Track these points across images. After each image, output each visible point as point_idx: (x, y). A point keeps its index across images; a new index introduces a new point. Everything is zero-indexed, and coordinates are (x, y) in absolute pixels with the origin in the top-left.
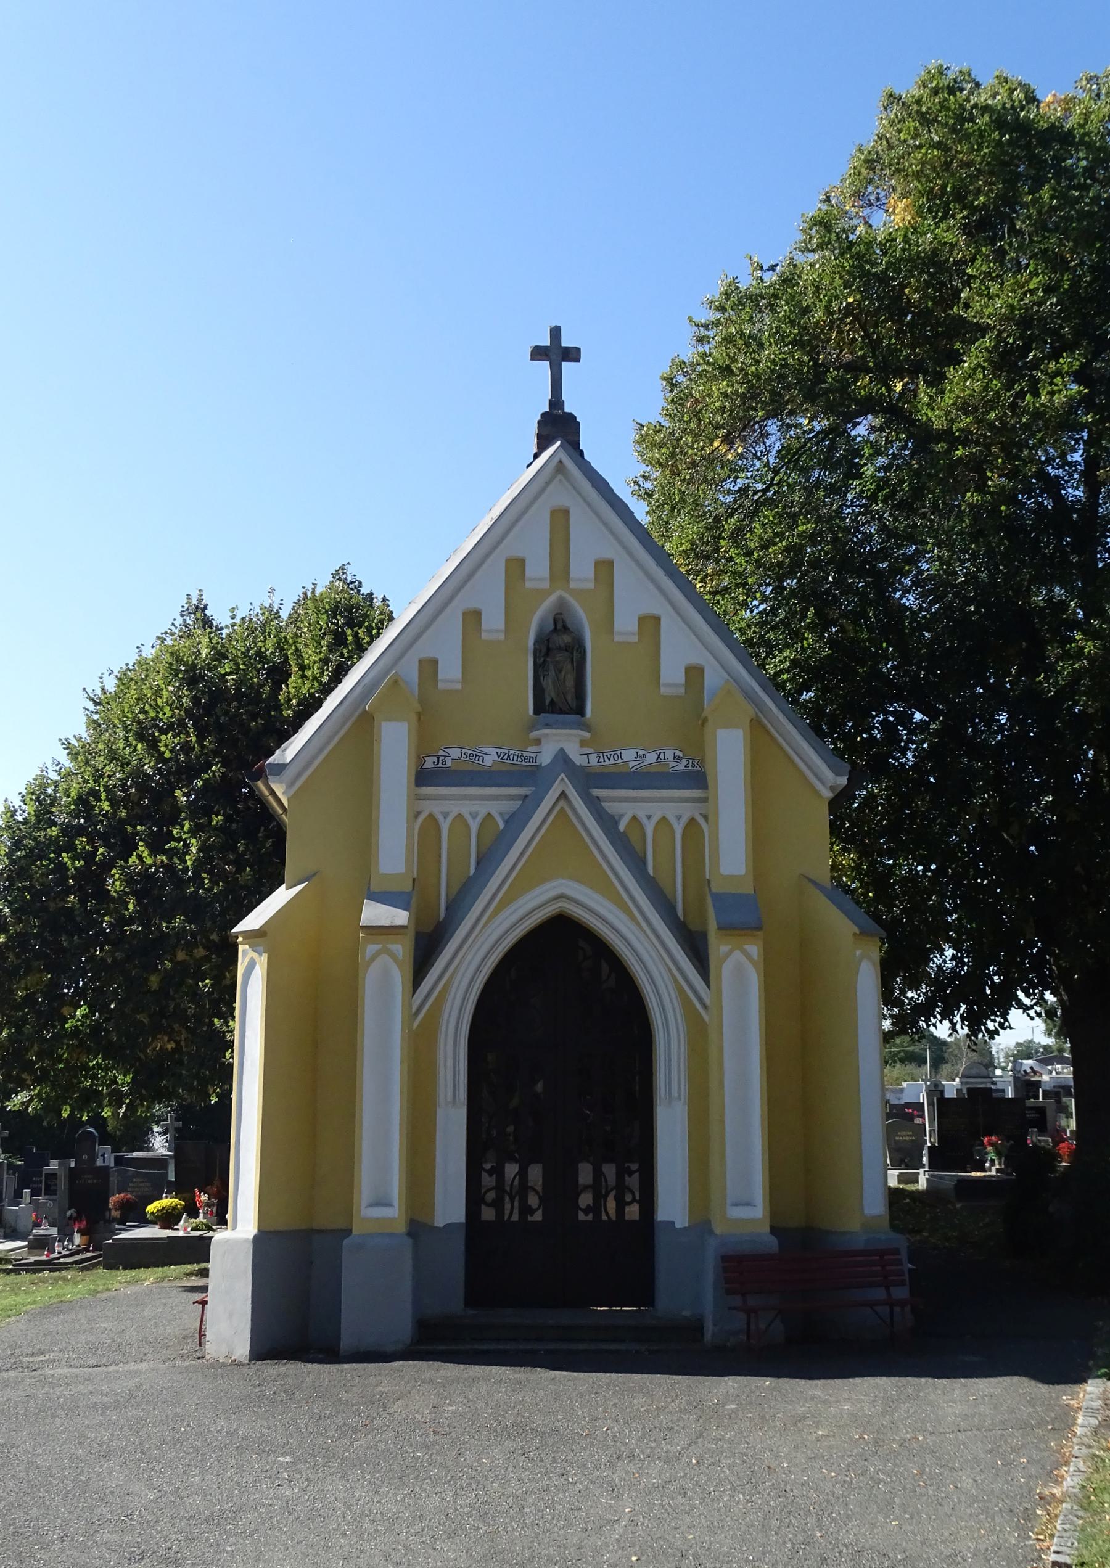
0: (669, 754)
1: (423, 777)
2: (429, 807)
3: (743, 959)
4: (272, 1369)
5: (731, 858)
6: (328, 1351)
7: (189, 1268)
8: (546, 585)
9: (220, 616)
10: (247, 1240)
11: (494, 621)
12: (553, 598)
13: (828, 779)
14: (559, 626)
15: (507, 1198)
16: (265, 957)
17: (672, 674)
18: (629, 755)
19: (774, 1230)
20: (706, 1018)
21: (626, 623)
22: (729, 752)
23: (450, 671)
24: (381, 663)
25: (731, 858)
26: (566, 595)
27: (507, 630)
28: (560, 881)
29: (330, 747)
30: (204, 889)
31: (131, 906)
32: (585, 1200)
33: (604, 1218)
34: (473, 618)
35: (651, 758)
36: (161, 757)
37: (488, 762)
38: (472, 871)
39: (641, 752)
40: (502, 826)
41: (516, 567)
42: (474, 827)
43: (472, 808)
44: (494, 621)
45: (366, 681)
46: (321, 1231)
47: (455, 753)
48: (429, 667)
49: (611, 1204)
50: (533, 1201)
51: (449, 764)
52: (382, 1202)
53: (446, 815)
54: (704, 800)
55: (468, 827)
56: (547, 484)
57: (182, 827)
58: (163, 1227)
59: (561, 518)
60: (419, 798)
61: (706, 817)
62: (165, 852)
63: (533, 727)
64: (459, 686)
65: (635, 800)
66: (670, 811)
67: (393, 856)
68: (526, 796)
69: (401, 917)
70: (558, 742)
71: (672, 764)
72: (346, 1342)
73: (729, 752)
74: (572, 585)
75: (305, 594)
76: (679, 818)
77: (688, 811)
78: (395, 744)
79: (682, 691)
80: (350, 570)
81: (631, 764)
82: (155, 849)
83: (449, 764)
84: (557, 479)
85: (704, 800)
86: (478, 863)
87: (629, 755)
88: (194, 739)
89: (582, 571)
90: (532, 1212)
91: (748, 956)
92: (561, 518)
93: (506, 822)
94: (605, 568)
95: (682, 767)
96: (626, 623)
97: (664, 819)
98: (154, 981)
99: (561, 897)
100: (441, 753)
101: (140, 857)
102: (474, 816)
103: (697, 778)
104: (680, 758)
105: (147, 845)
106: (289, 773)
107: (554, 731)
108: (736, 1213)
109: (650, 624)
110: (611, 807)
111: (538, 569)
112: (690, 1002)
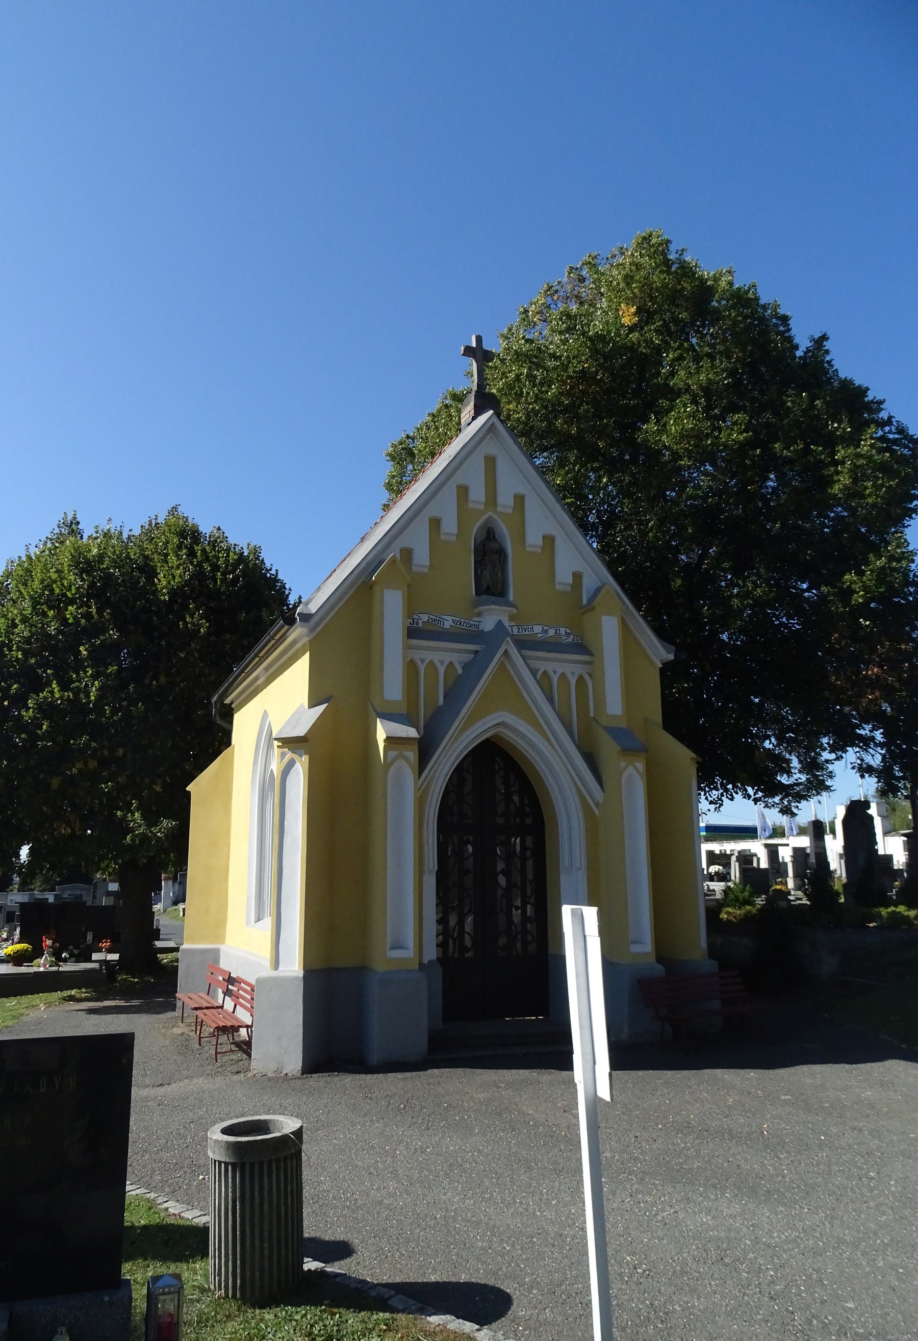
0: (563, 631)
1: (413, 632)
2: (417, 655)
3: (635, 772)
4: (318, 1080)
5: (614, 705)
6: (358, 1064)
7: (59, 994)
8: (482, 507)
9: (87, 529)
10: (297, 978)
11: (450, 526)
12: (486, 516)
13: (660, 653)
14: (491, 537)
15: (451, 940)
16: (305, 758)
17: (564, 577)
18: (538, 629)
19: (659, 959)
20: (597, 812)
21: (534, 538)
22: (609, 630)
23: (422, 558)
24: (378, 548)
25: (614, 705)
26: (495, 517)
27: (458, 536)
28: (501, 713)
29: (340, 604)
30: (106, 718)
31: (44, 727)
32: (502, 941)
33: (514, 953)
34: (435, 523)
35: (552, 632)
36: (64, 621)
37: (447, 625)
38: (441, 701)
39: (545, 628)
40: (460, 671)
41: (463, 492)
42: (442, 670)
43: (444, 657)
44: (450, 526)
45: (369, 558)
46: (337, 969)
47: (425, 618)
48: (407, 554)
49: (519, 945)
50: (468, 942)
51: (420, 625)
52: (397, 946)
53: (422, 661)
54: (590, 663)
55: (437, 671)
56: (482, 439)
57: (86, 672)
58: (15, 965)
59: (491, 462)
60: (410, 647)
61: (590, 675)
62: (72, 690)
63: (476, 604)
64: (426, 570)
65: (546, 659)
66: (567, 669)
67: (393, 688)
68: (476, 652)
69: (412, 732)
70: (491, 618)
71: (565, 638)
72: (374, 1058)
73: (609, 630)
74: (499, 509)
75: (151, 521)
76: (573, 674)
77: (579, 670)
78: (392, 607)
79: (569, 589)
80: (180, 509)
81: (539, 636)
82: (64, 687)
83: (420, 625)
84: (488, 437)
85: (590, 663)
86: (445, 697)
87: (538, 629)
88: (95, 611)
89: (505, 500)
90: (467, 950)
91: (637, 770)
92: (491, 462)
93: (463, 668)
94: (520, 500)
95: (570, 640)
96: (534, 538)
97: (563, 674)
98: (55, 782)
99: (502, 724)
100: (415, 616)
101: (52, 692)
102: (442, 662)
103: (581, 647)
104: (569, 634)
105: (58, 684)
106: (314, 621)
107: (497, 607)
108: (634, 949)
109: (549, 541)
110: (535, 664)
111: (478, 494)
112: (586, 800)
